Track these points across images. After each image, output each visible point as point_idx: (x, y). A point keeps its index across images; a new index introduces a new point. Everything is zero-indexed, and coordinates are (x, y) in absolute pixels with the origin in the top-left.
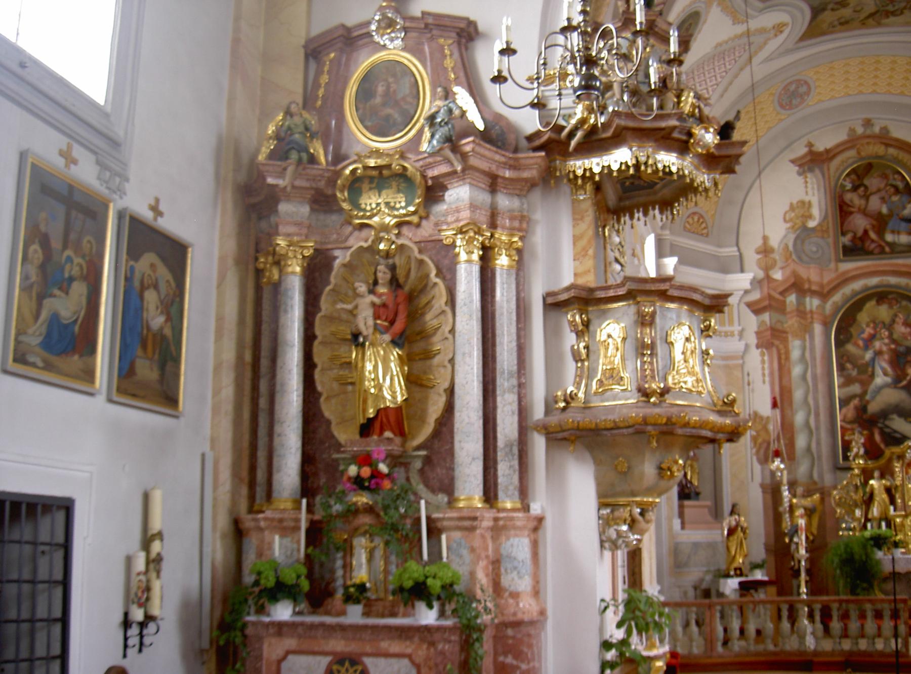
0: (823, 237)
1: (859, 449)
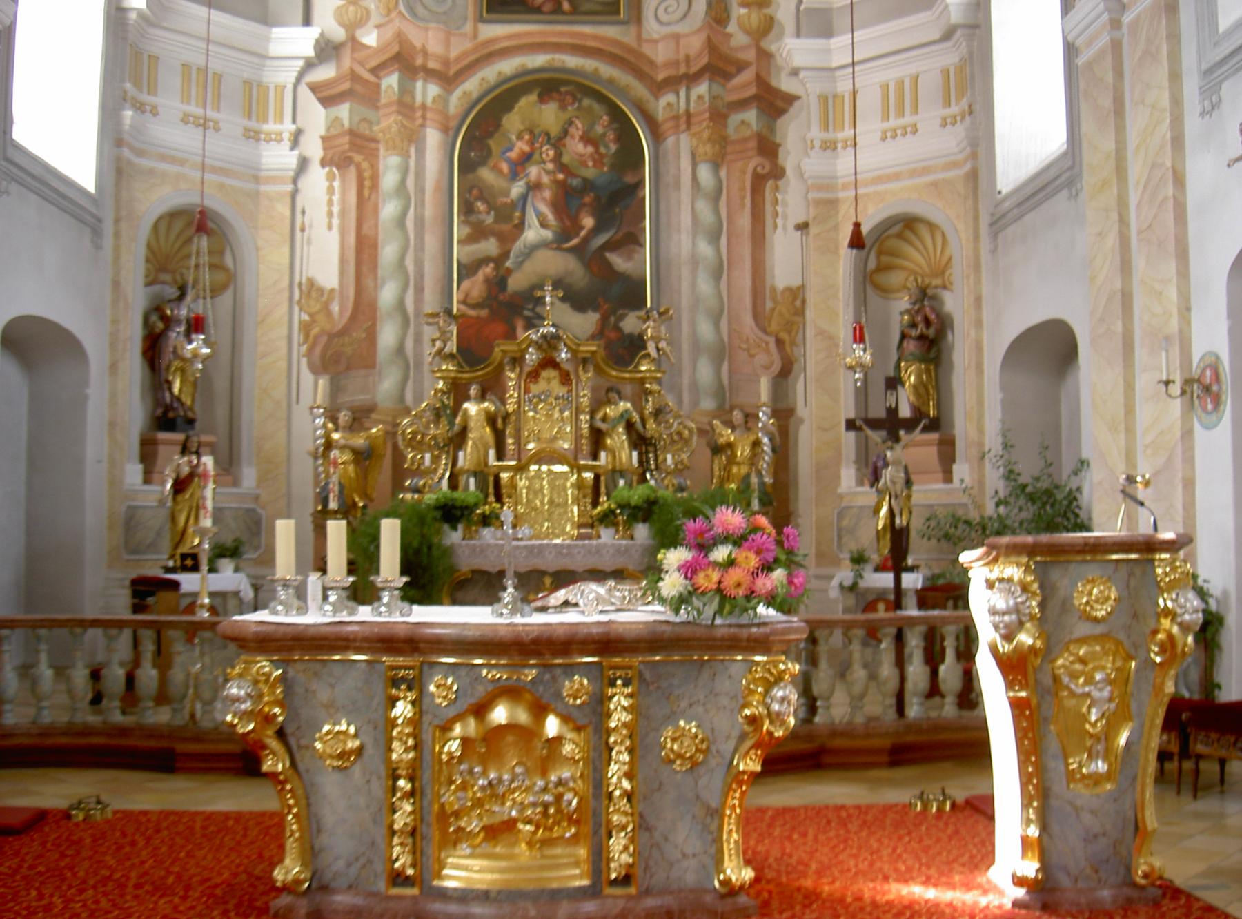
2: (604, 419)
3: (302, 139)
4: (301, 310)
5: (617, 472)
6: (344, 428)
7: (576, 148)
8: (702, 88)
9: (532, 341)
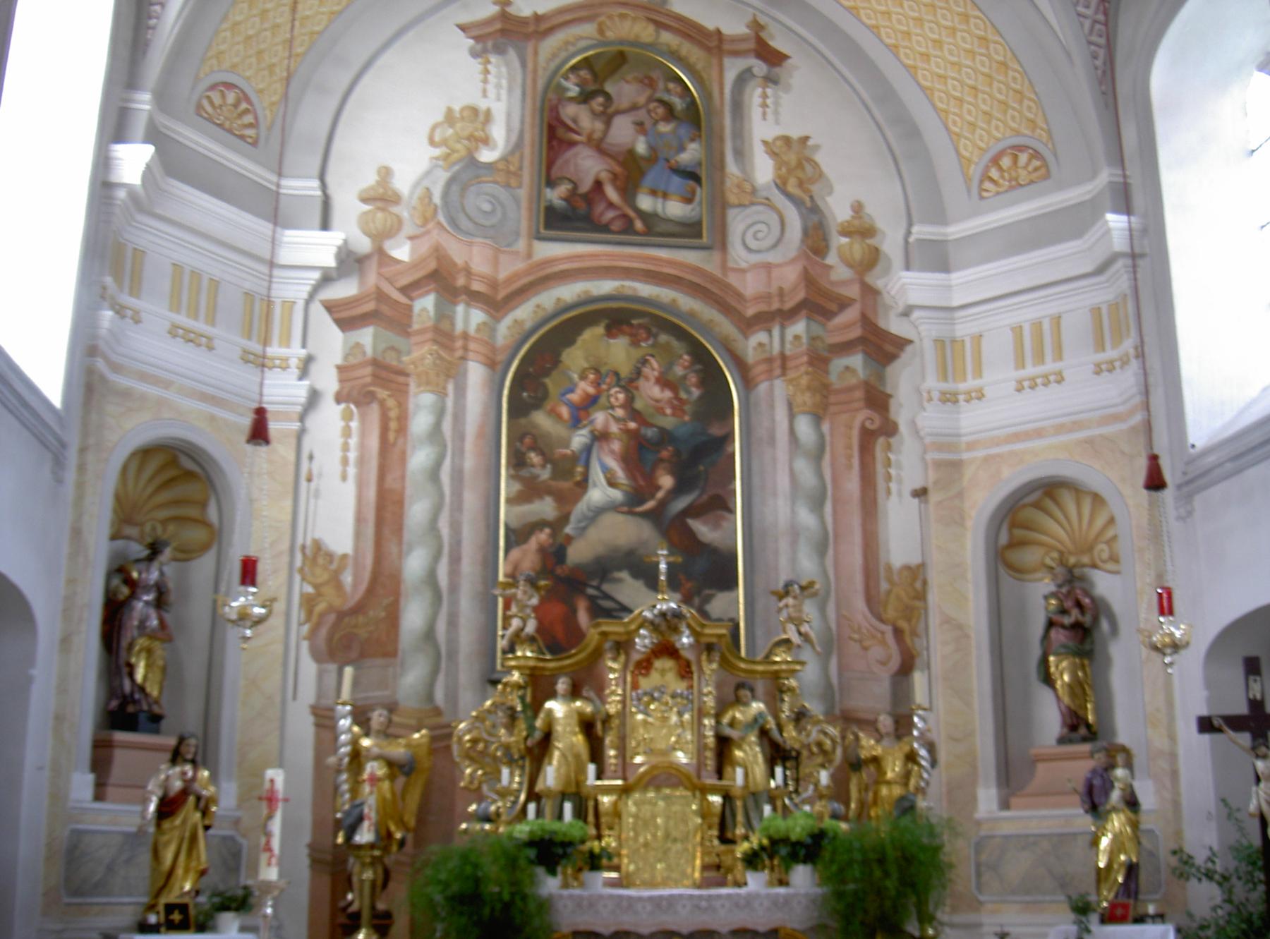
0: (507, 186)
1: (524, 621)
2: (732, 724)
3: (314, 368)
4: (303, 579)
5: (755, 797)
6: (378, 732)
7: (651, 391)
8: (799, 328)
9: (645, 620)
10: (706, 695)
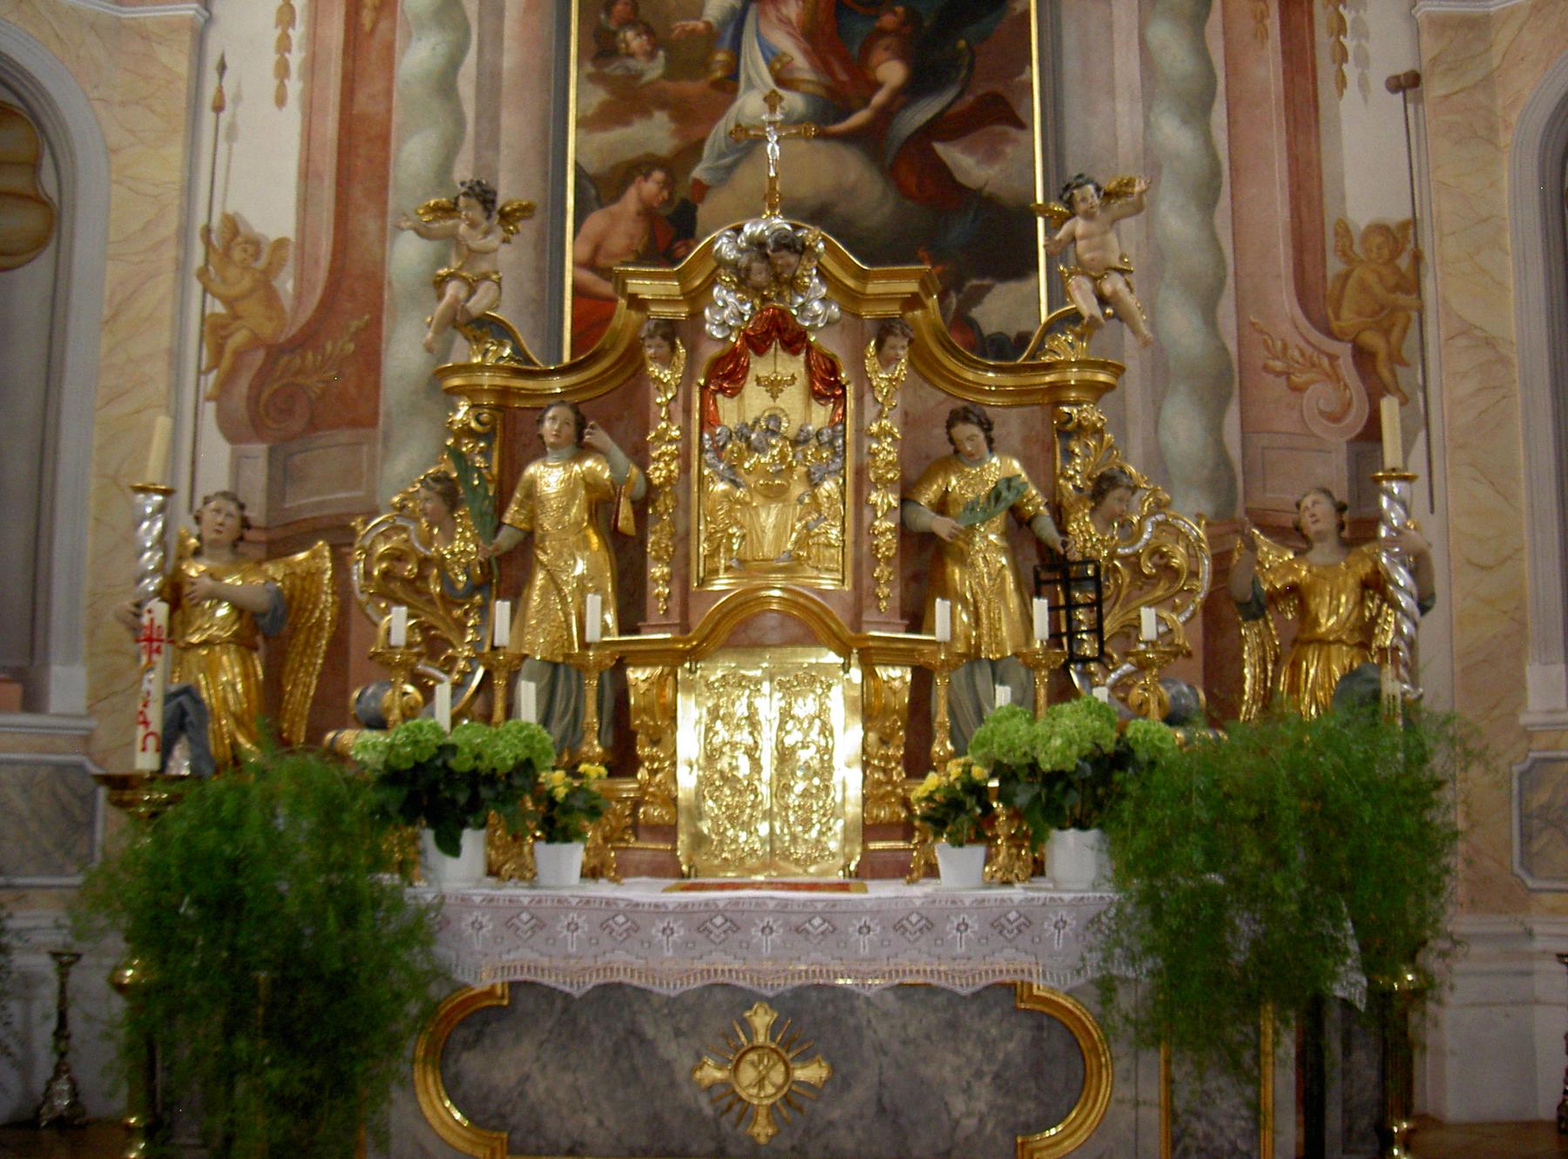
2: (942, 506)
9: (722, 263)
10: (876, 437)
